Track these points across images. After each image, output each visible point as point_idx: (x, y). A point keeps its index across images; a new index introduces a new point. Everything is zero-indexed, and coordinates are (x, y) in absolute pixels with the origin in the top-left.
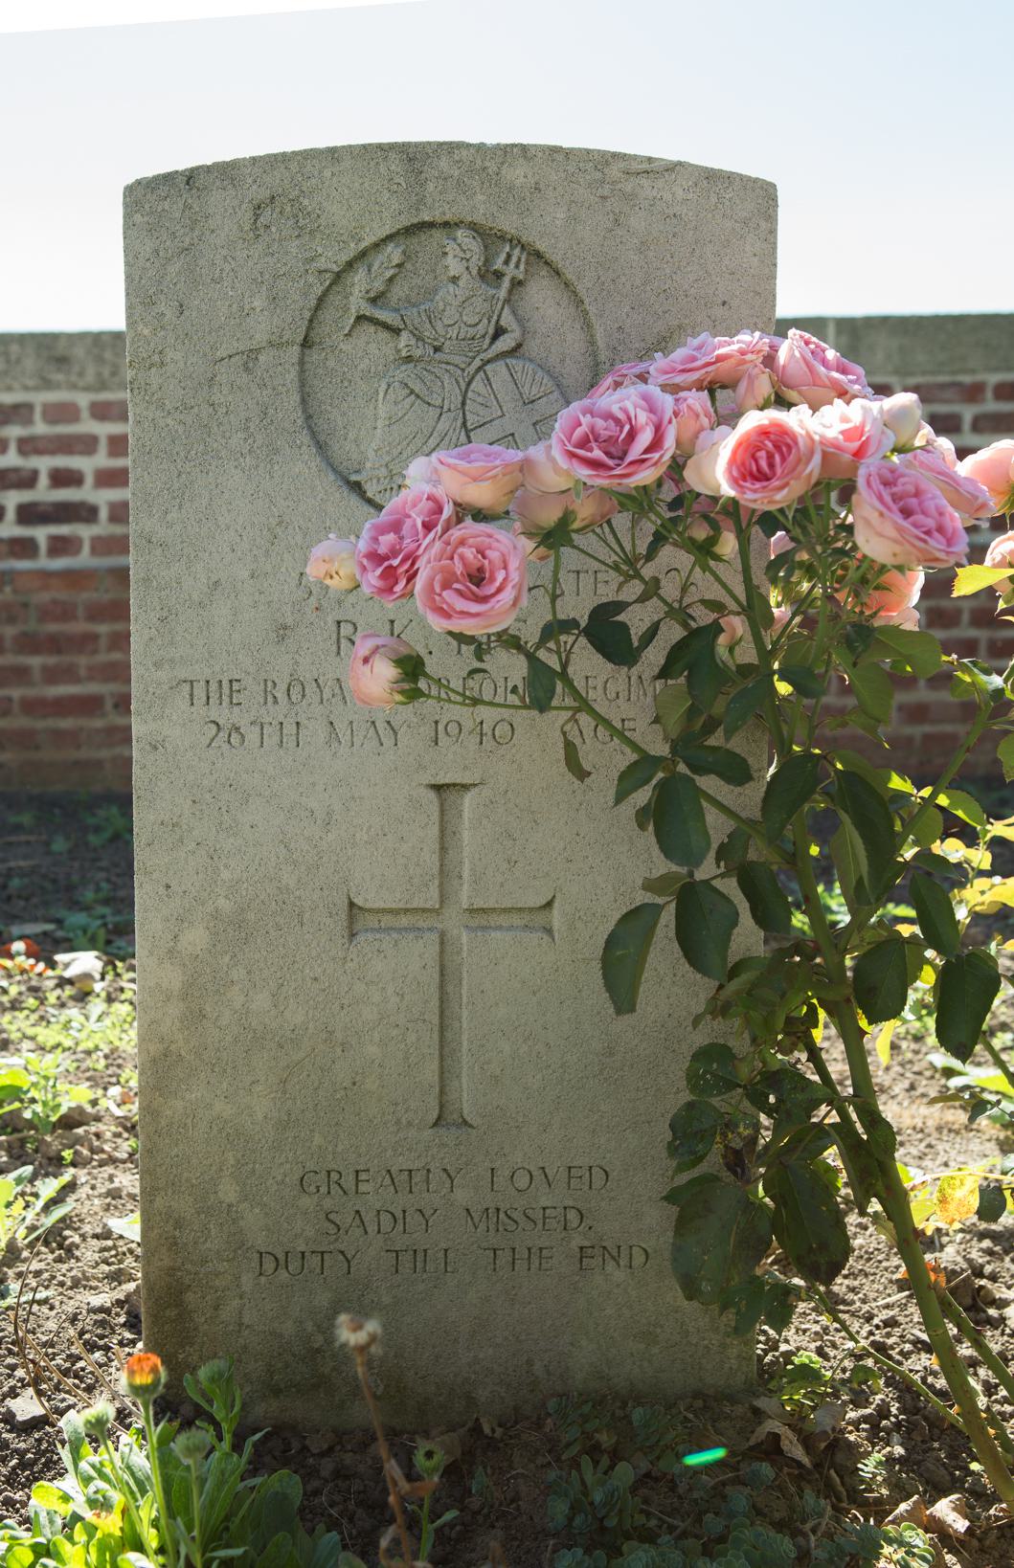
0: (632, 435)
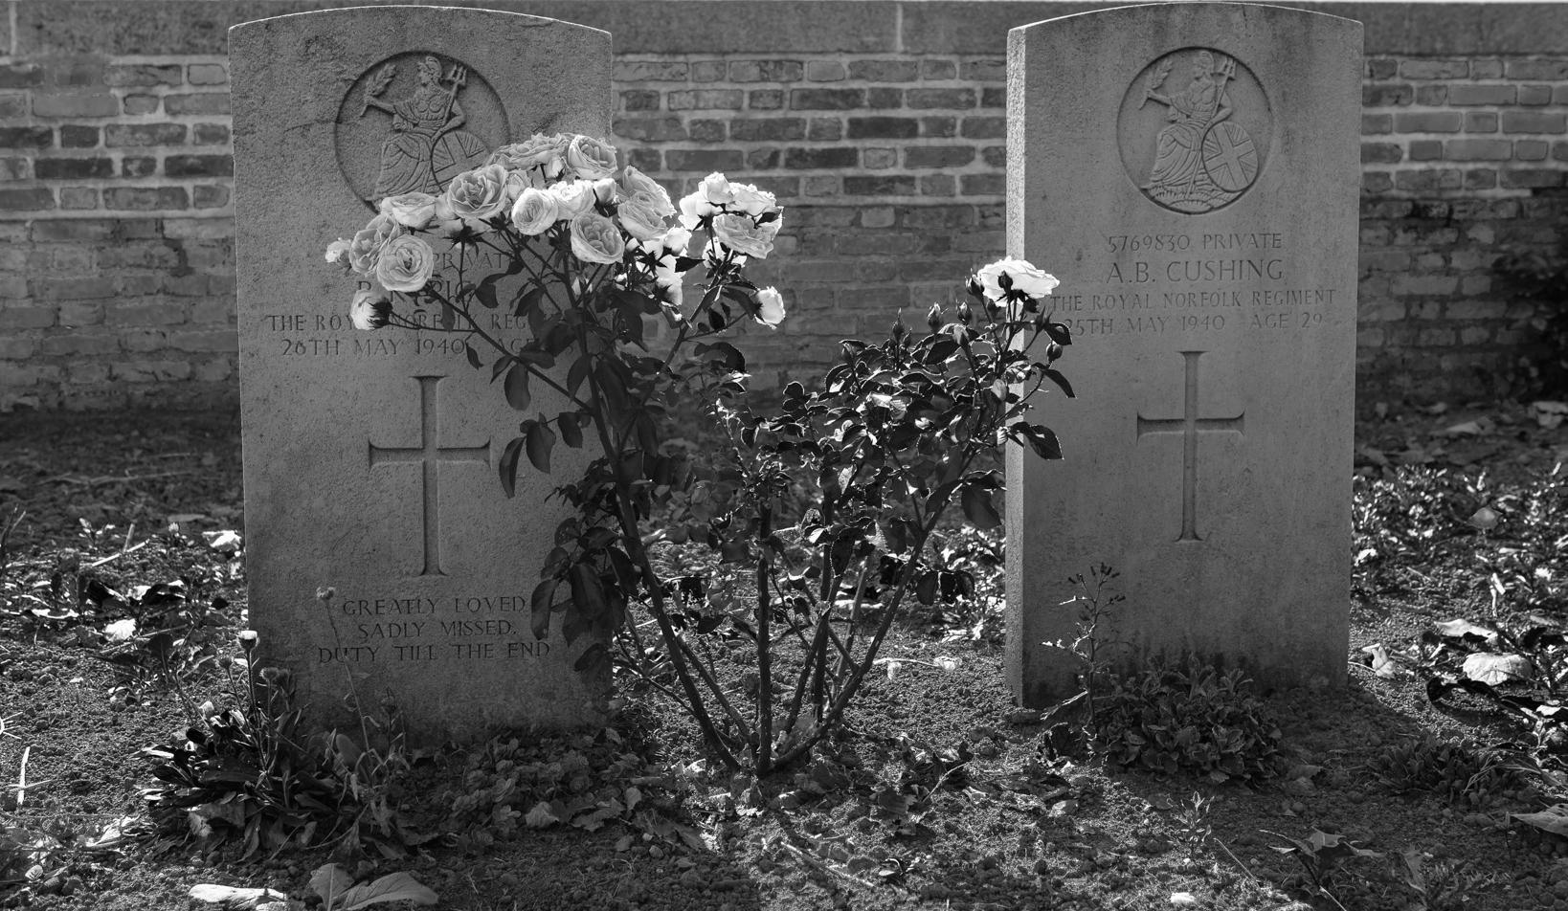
0: (486, 192)
